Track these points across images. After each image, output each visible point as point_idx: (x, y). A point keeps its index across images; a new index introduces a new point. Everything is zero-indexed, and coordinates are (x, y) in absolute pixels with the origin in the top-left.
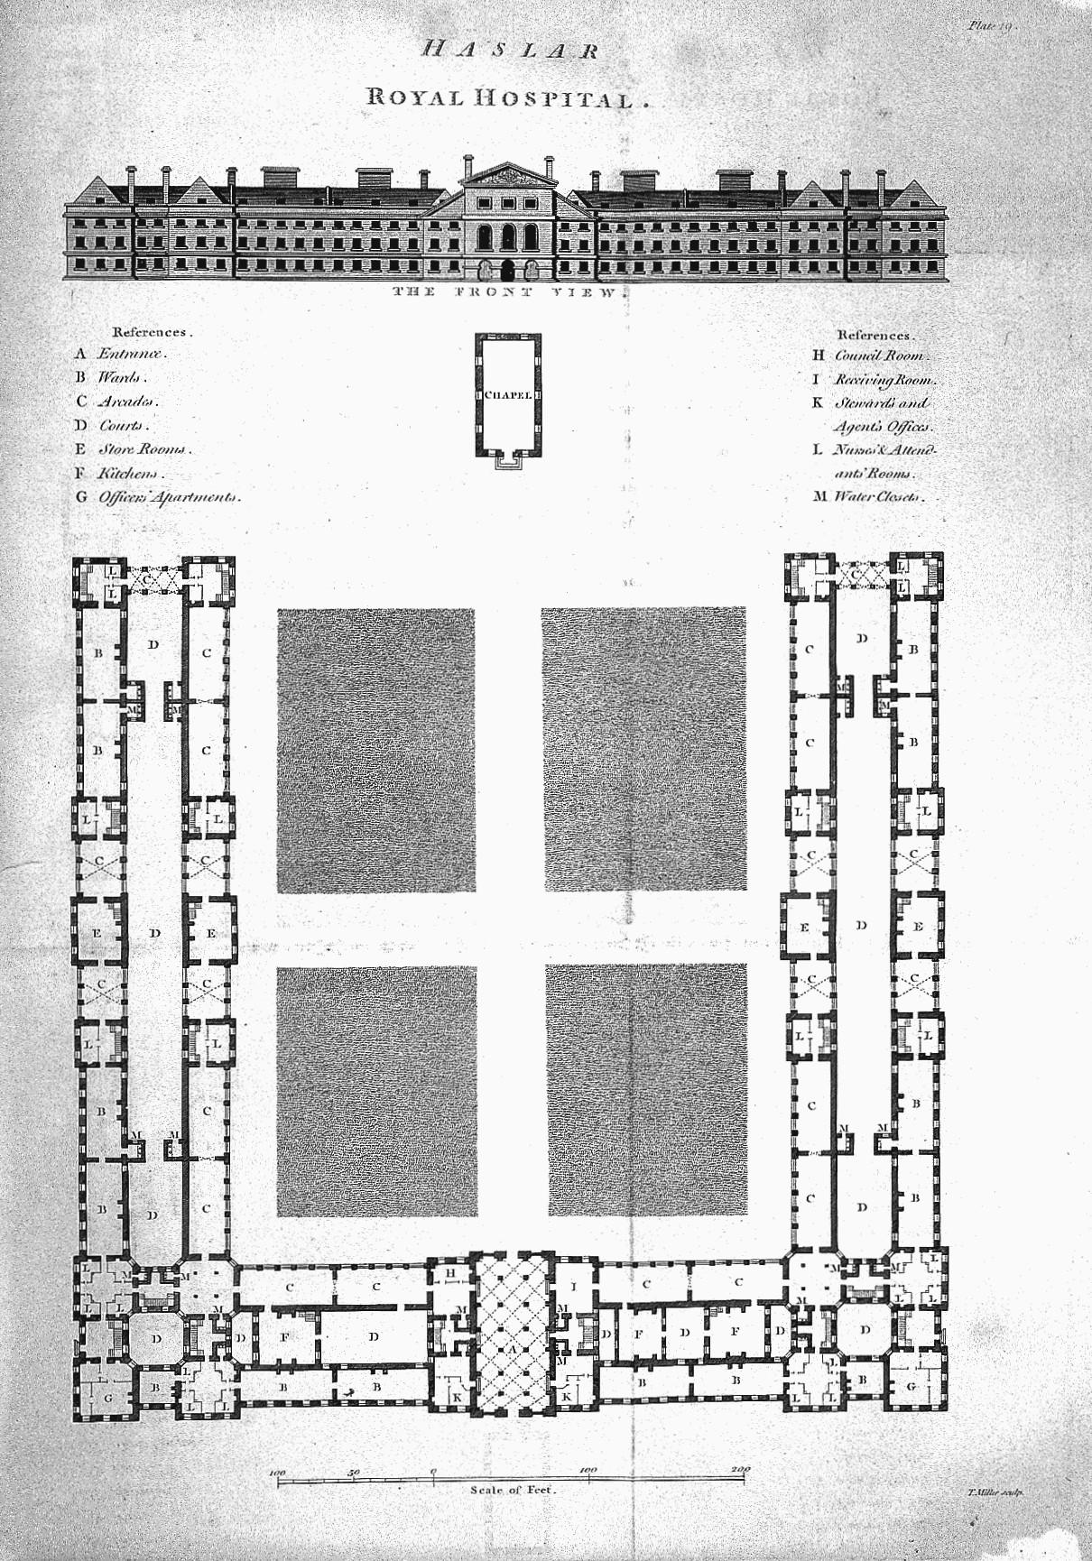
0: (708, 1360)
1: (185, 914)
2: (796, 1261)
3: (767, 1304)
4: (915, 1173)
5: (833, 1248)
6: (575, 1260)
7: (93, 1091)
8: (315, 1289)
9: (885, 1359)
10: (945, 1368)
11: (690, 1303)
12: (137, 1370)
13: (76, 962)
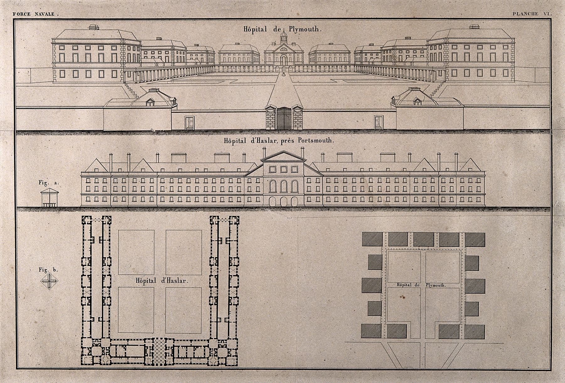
0: (194, 358)
1: (229, 278)
2: (109, 340)
3: (204, 347)
4: (106, 324)
5: (217, 338)
6: (170, 339)
7: (84, 310)
8: (125, 343)
9: (226, 358)
10: (237, 359)
11: (191, 346)
12: (93, 357)
13: (82, 287)
